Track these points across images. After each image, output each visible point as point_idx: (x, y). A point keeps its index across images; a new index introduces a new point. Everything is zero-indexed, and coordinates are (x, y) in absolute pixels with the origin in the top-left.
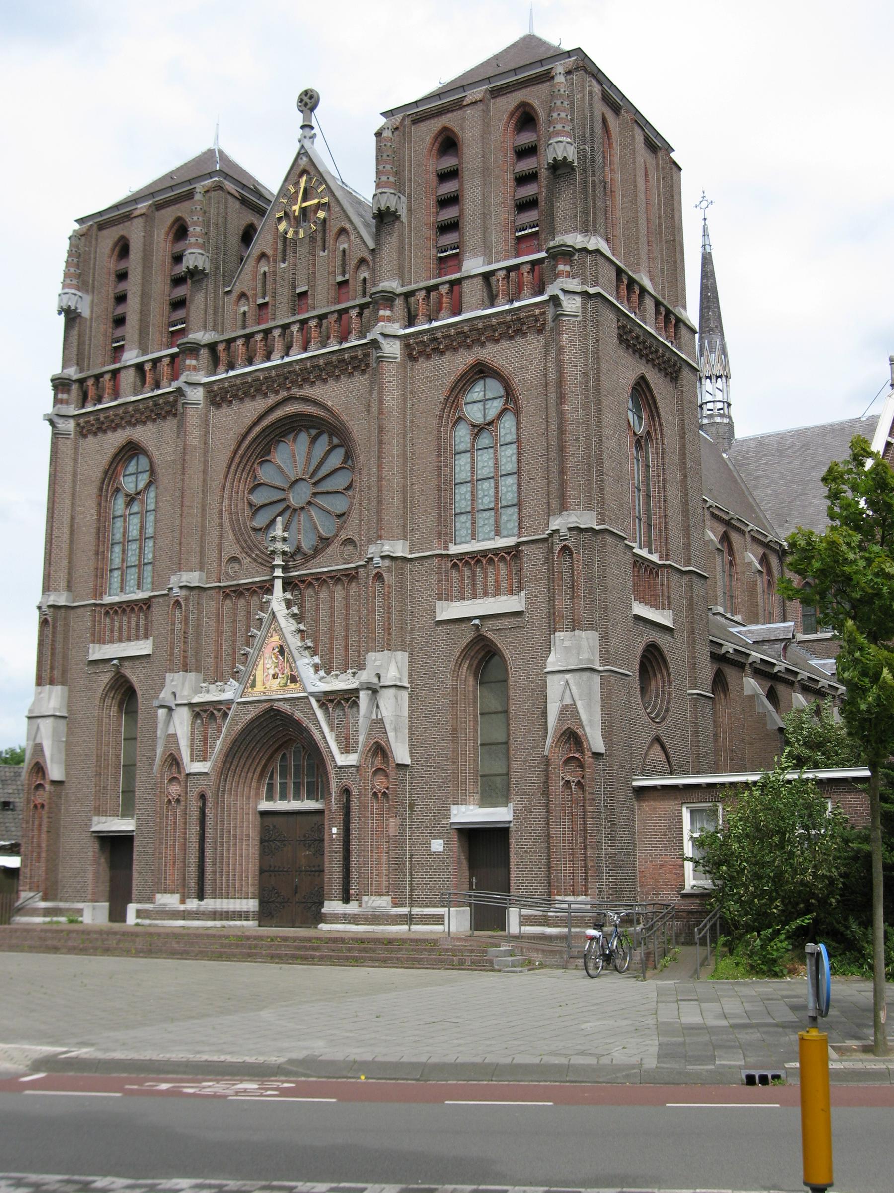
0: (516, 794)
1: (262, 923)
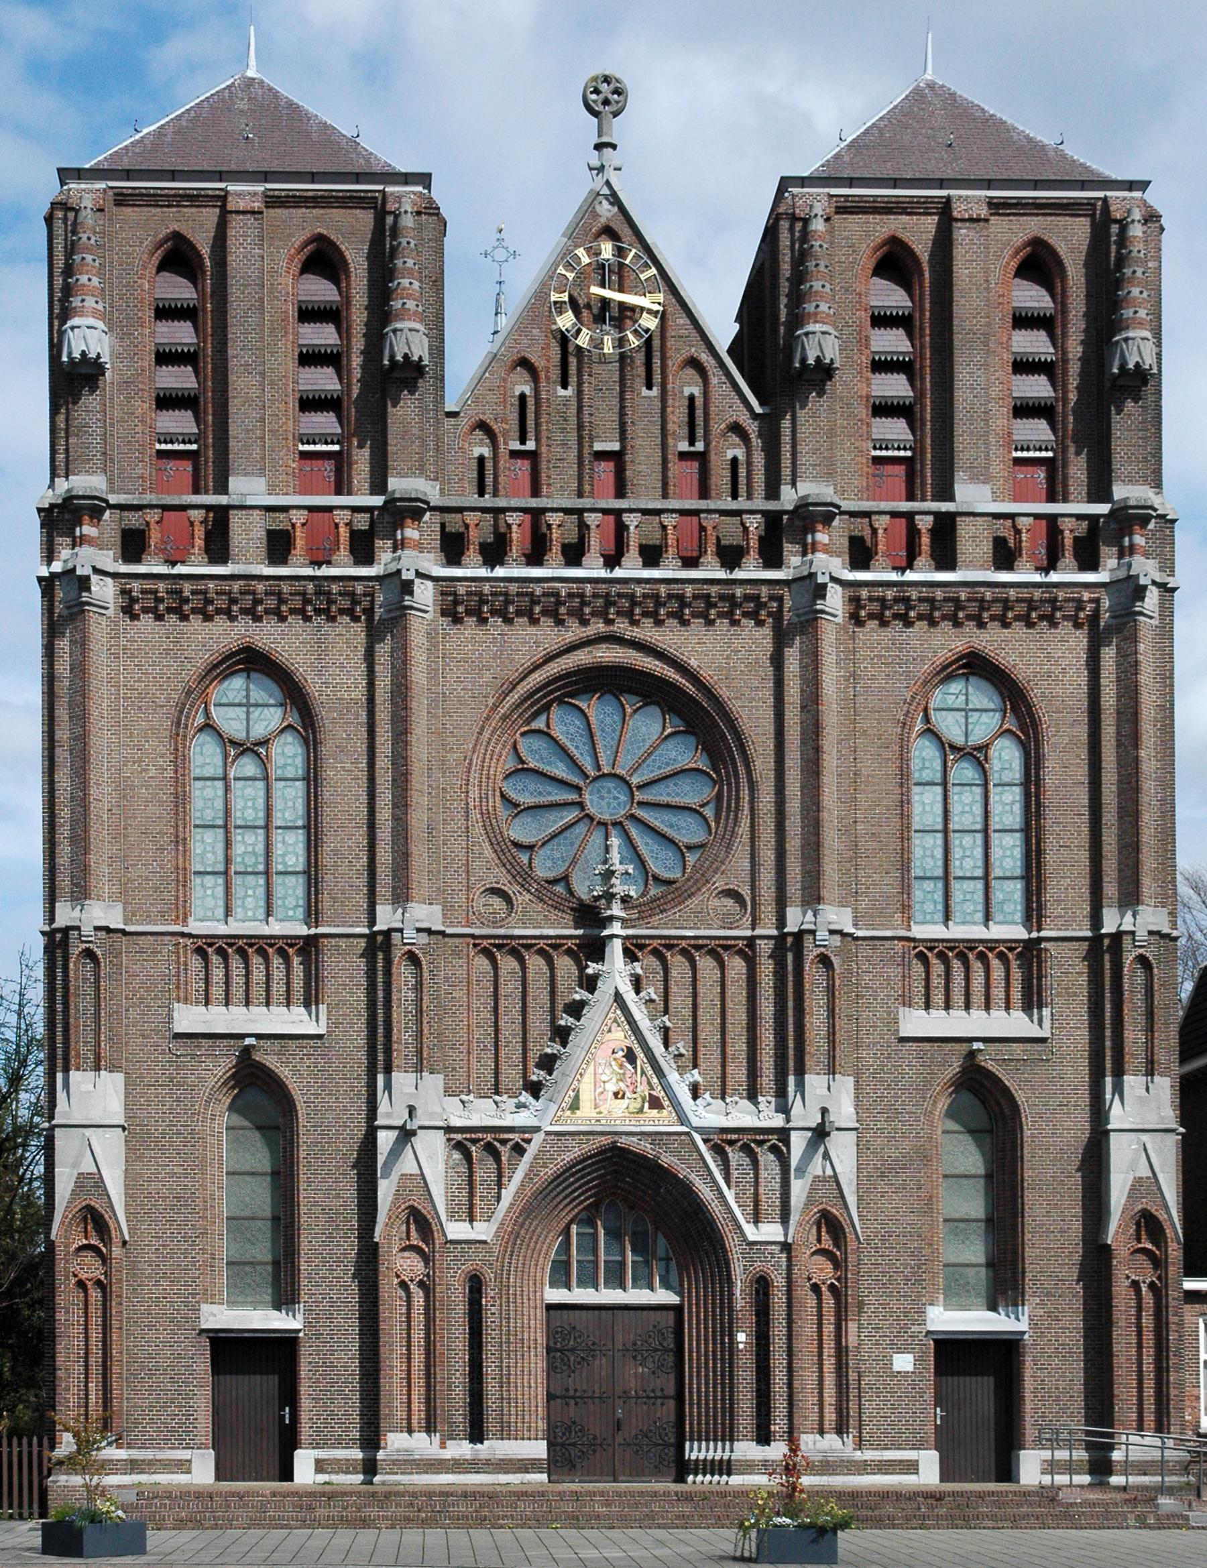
1: (553, 1477)
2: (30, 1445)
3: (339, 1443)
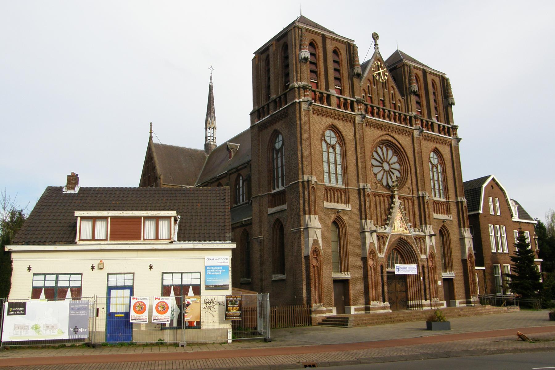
3: (360, 304)
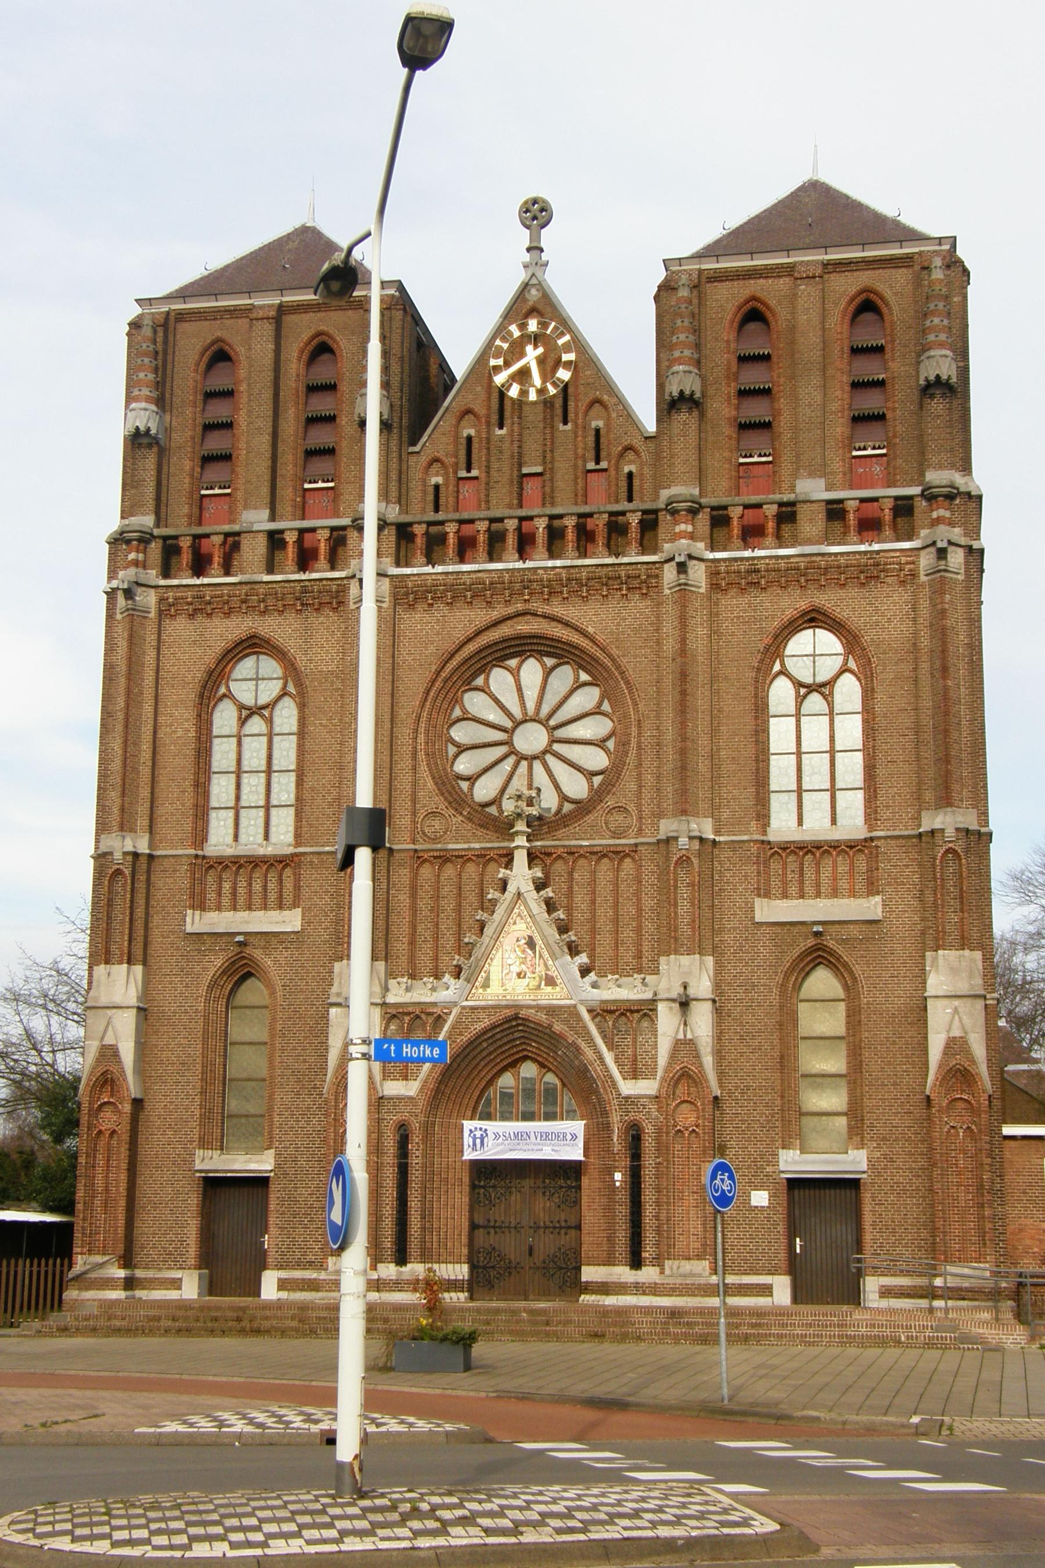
0: (872, 1139)
2: (39, 1265)
